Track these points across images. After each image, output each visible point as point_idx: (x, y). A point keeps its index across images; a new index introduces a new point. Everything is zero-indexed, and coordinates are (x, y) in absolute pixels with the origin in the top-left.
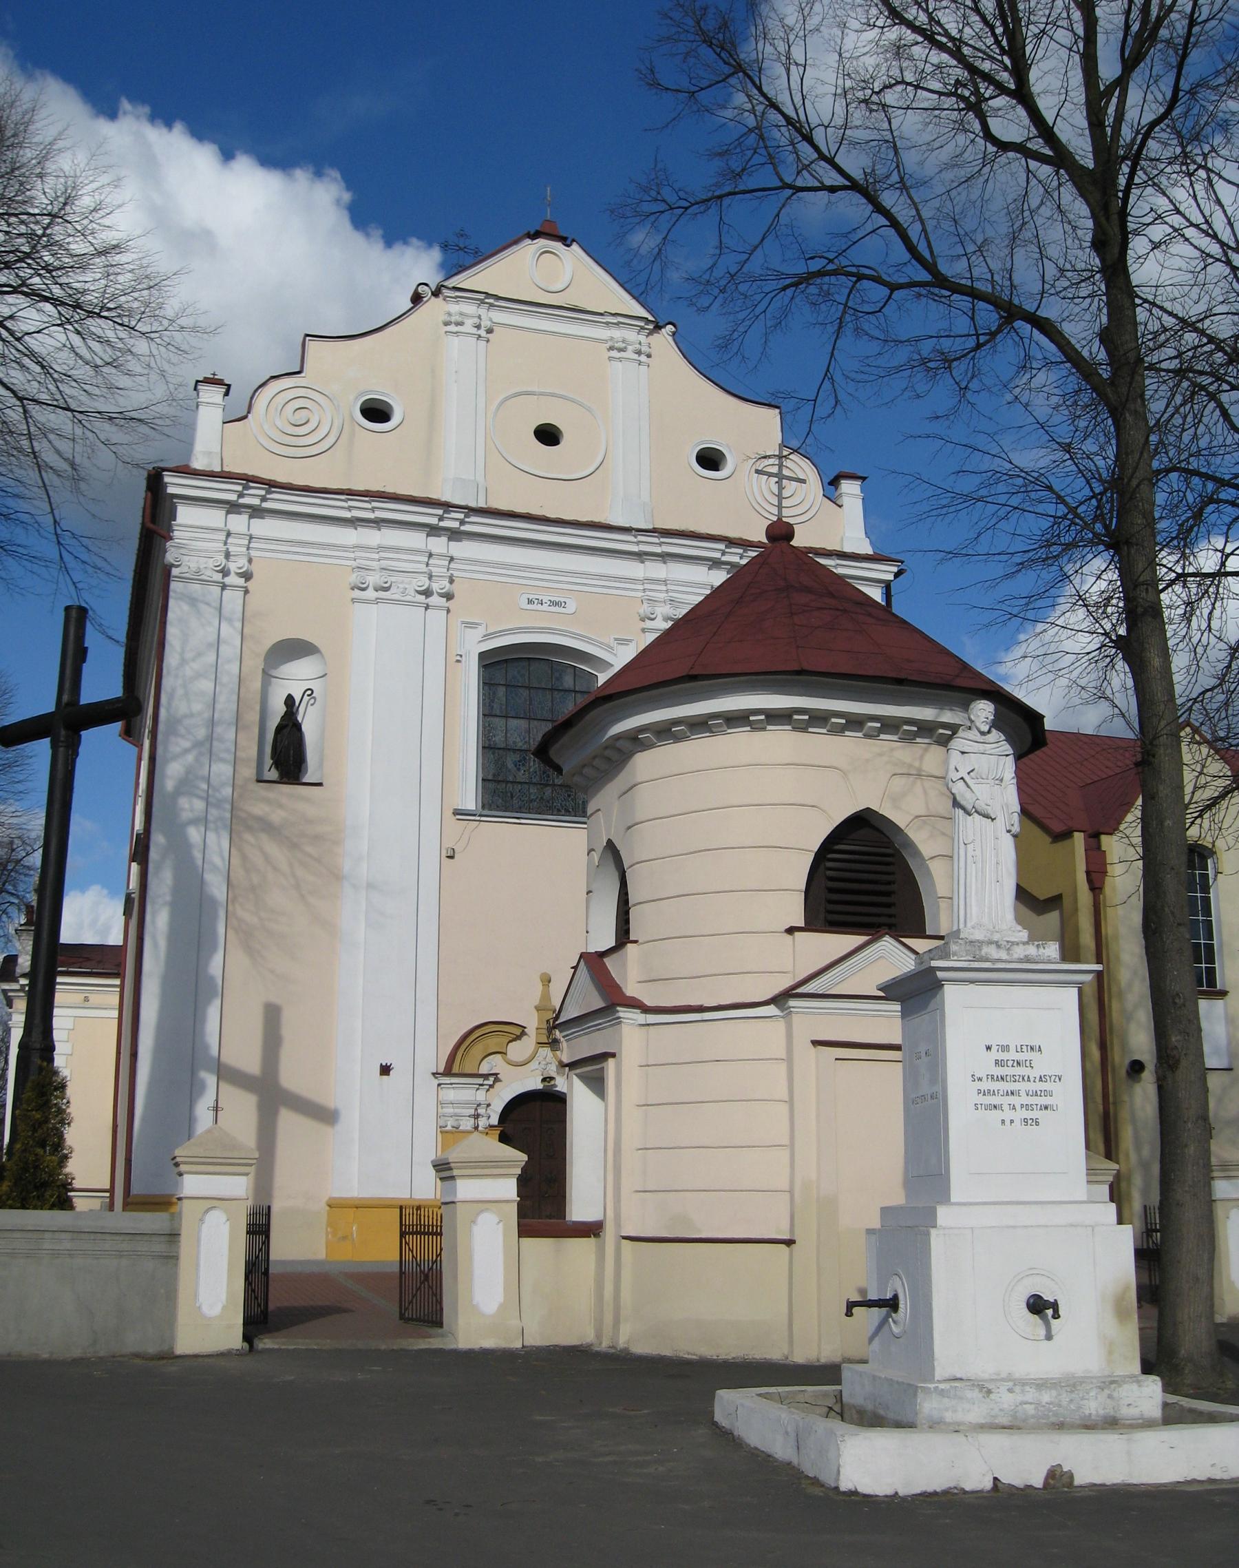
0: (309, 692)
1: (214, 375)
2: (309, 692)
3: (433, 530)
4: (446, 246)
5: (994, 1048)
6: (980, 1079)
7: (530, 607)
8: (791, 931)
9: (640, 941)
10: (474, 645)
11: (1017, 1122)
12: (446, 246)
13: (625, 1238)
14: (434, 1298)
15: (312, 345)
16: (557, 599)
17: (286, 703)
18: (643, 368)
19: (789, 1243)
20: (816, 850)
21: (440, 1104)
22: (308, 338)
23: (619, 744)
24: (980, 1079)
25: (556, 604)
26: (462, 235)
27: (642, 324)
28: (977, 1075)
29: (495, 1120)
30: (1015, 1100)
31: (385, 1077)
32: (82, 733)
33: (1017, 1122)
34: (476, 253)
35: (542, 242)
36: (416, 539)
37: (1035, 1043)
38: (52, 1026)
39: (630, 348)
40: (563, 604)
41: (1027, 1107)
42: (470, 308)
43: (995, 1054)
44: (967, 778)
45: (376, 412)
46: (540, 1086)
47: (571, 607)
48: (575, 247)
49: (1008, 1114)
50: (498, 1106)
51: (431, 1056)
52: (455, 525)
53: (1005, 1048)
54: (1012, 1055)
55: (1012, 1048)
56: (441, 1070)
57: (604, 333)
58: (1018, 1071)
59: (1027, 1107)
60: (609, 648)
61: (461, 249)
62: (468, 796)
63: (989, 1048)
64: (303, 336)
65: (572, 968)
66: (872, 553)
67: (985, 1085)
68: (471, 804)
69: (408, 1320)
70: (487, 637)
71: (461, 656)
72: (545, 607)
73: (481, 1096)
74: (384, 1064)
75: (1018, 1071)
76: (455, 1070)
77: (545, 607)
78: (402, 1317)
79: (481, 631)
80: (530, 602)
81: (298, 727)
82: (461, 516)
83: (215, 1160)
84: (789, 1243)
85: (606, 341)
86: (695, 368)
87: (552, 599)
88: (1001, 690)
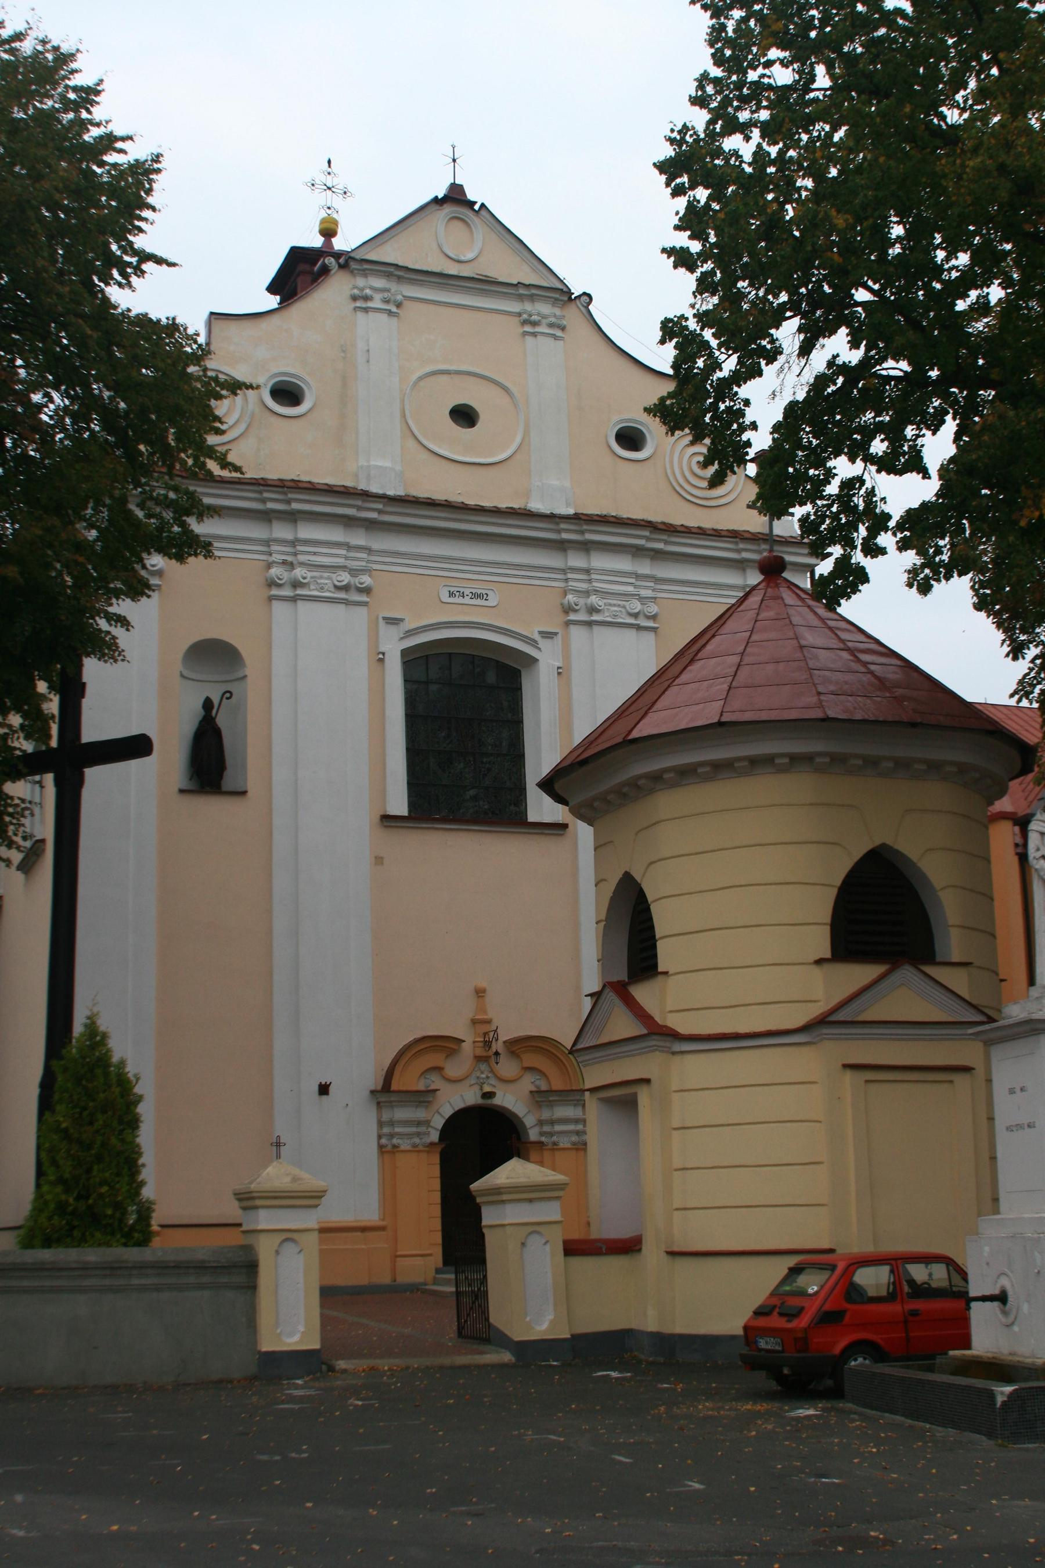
0: (228, 695)
2: (228, 695)
3: (348, 522)
7: (451, 600)
8: (819, 962)
9: (670, 973)
12: (313, 185)
15: (217, 325)
16: (479, 592)
18: (560, 343)
21: (381, 1124)
22: (213, 317)
23: (641, 782)
25: (479, 596)
26: (329, 173)
27: (557, 296)
29: (435, 1137)
31: (324, 1097)
32: (85, 770)
34: (345, 193)
36: (336, 534)
38: (453, 1114)
39: (544, 321)
40: (485, 596)
42: (379, 283)
46: (480, 1101)
47: (492, 601)
50: (439, 1122)
51: (370, 1076)
56: (379, 1088)
57: (514, 307)
60: (533, 643)
65: (591, 995)
69: (466, 1337)
70: (410, 633)
71: (383, 654)
72: (467, 600)
73: (420, 1114)
74: (323, 1083)
76: (394, 1087)
77: (467, 600)
78: (460, 1334)
81: (217, 733)
83: (292, 1194)
85: (519, 314)
87: (474, 591)
88: (1004, 730)
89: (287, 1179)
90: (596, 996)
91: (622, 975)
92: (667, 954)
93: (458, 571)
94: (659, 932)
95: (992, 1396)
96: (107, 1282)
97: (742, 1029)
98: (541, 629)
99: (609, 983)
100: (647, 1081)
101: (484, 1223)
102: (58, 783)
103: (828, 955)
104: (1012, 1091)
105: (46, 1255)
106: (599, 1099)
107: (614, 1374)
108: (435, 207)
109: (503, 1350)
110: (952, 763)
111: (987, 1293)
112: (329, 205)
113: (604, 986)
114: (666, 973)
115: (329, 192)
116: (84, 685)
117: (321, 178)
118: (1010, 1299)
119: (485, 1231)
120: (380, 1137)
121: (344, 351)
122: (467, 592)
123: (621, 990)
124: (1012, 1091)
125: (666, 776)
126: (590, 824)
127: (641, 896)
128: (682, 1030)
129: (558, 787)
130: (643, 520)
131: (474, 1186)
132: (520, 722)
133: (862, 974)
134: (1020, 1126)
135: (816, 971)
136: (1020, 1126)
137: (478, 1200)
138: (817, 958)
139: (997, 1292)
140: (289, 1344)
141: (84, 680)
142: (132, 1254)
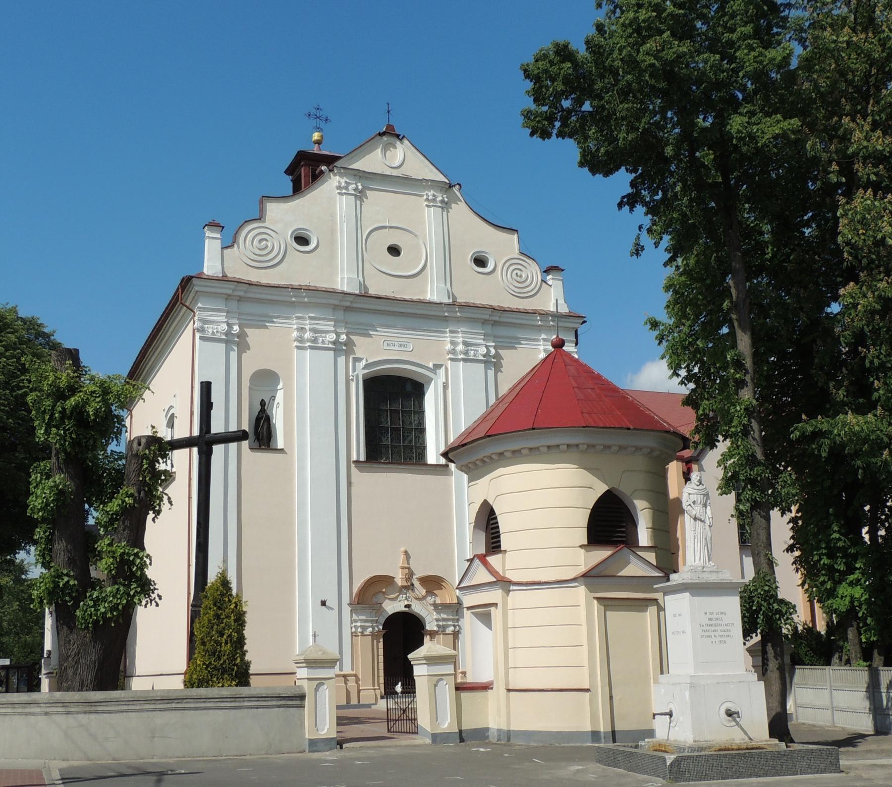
0: (273, 398)
1: (214, 220)
2: (273, 398)
4: (309, 115)
5: (708, 613)
6: (703, 626)
10: (361, 371)
11: (717, 642)
13: (588, 690)
14: (413, 726)
17: (261, 404)
19: (509, 690)
20: (591, 508)
24: (703, 626)
25: (403, 346)
28: (702, 624)
30: (717, 634)
33: (717, 642)
34: (327, 120)
35: (385, 138)
37: (723, 611)
41: (721, 636)
43: (709, 616)
44: (692, 505)
45: (302, 240)
48: (406, 142)
49: (714, 639)
50: (383, 620)
52: (348, 304)
53: (712, 613)
54: (715, 616)
55: (715, 614)
58: (717, 622)
59: (721, 636)
61: (317, 117)
62: (358, 451)
63: (706, 613)
64: (261, 196)
65: (468, 560)
66: (567, 311)
67: (705, 628)
68: (362, 458)
75: (717, 622)
77: (396, 348)
79: (364, 363)
80: (388, 345)
81: (268, 419)
82: (351, 299)
84: (509, 690)
86: (437, 168)
87: (400, 343)
89: (320, 653)
90: (471, 561)
91: (482, 550)
92: (505, 542)
93: (391, 333)
94: (502, 529)
95: (665, 760)
96: (233, 704)
97: (543, 579)
98: (435, 363)
99: (477, 555)
100: (496, 604)
101: (415, 674)
102: (199, 453)
103: (586, 543)
104: (675, 616)
105: (202, 691)
106: (472, 613)
107: (482, 750)
108: (378, 137)
109: (564, 764)
110: (647, 447)
111: (663, 712)
112: (318, 126)
113: (474, 557)
114: (505, 551)
115: (318, 120)
116: (212, 403)
117: (313, 111)
118: (674, 714)
119: (415, 678)
120: (351, 628)
121: (332, 216)
122: (396, 343)
123: (482, 558)
124: (675, 616)
125: (506, 454)
126: (467, 474)
127: (492, 512)
128: (514, 579)
129: (450, 455)
130: (487, 305)
131: (409, 656)
132: (423, 412)
133: (601, 554)
134: (678, 632)
135: (582, 551)
136: (678, 632)
137: (412, 663)
138: (580, 544)
139: (668, 711)
140: (322, 735)
141: (212, 401)
142: (243, 691)
